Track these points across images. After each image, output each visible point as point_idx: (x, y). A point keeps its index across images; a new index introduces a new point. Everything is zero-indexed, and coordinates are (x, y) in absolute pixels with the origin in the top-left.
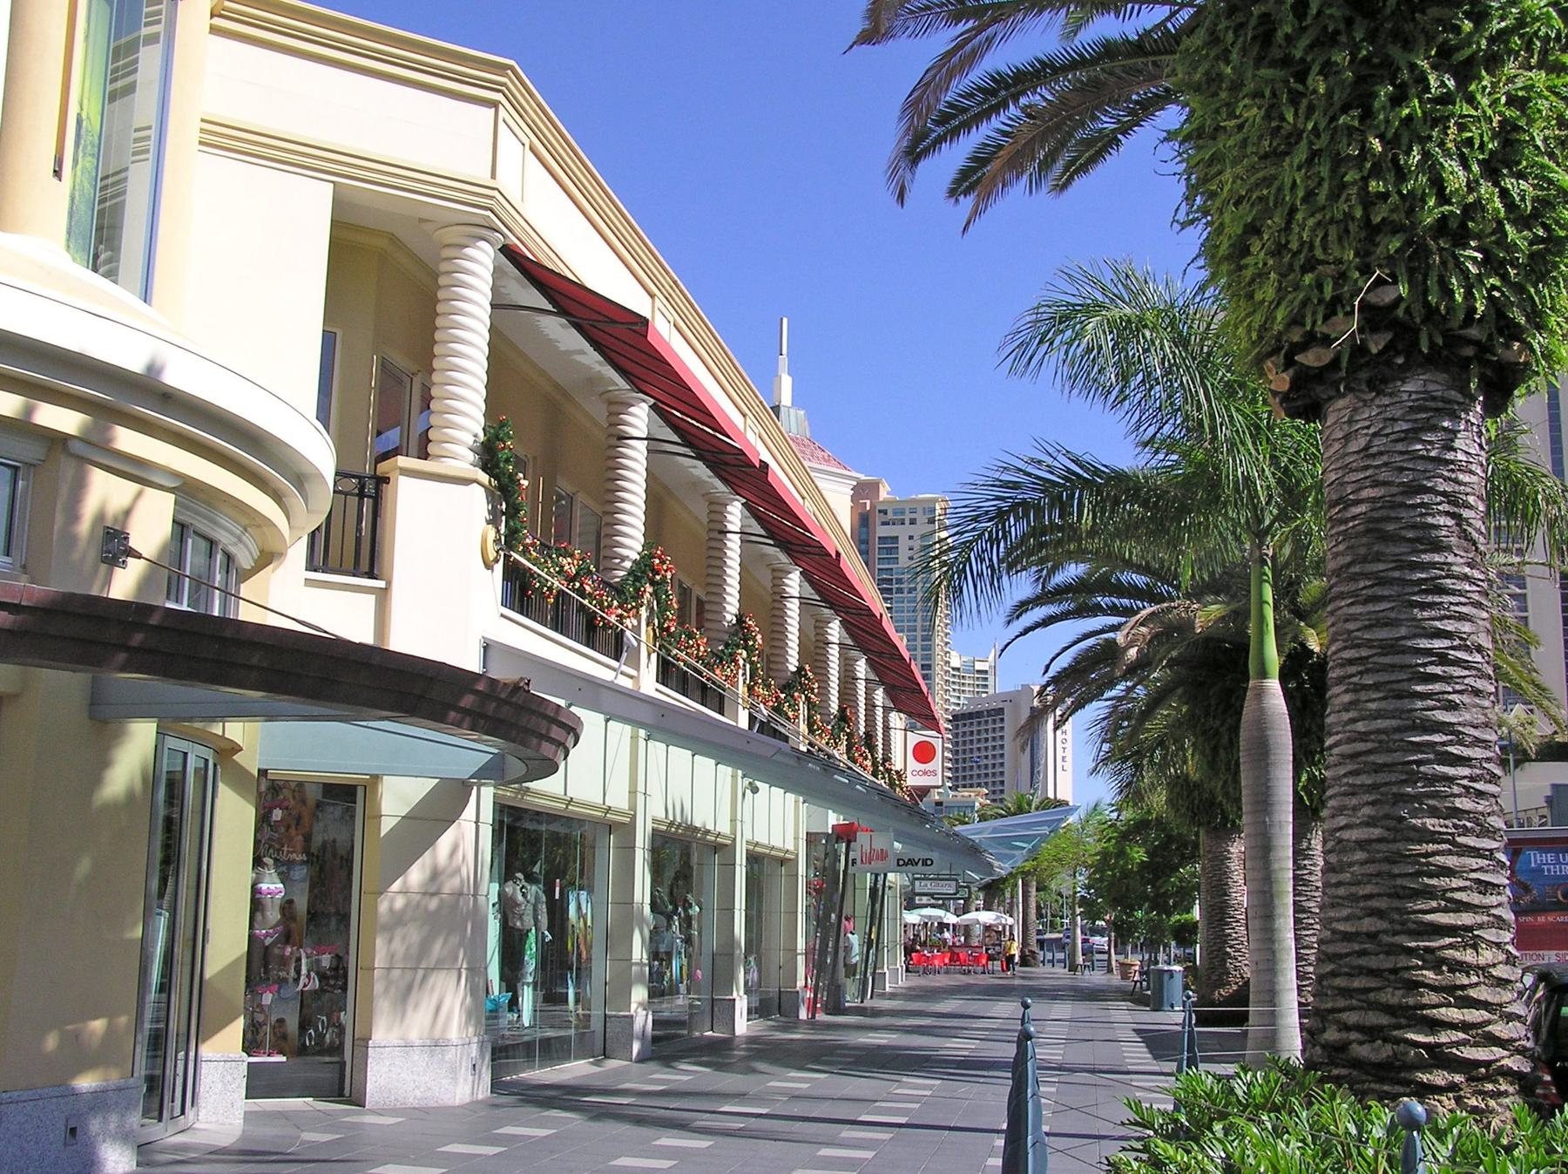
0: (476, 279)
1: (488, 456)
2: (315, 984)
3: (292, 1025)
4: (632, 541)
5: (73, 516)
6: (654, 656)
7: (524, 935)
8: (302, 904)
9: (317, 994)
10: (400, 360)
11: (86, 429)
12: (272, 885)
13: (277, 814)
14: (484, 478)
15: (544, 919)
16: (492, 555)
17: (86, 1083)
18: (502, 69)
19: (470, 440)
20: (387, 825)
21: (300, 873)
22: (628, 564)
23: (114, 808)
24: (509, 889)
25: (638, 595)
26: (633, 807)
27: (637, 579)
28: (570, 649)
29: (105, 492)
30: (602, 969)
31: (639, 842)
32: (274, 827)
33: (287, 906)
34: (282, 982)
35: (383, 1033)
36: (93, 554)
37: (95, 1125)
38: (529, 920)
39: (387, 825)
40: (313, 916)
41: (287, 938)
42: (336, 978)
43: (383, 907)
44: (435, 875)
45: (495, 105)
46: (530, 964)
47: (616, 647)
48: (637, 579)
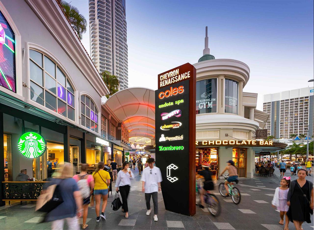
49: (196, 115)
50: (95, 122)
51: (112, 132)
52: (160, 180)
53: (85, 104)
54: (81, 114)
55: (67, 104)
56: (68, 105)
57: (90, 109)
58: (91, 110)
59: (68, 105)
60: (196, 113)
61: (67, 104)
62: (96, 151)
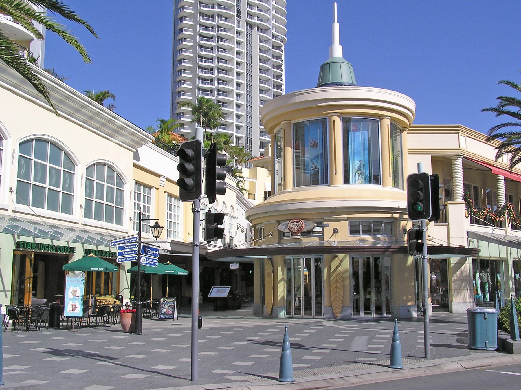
0: (459, 165)
1: (465, 198)
2: (443, 293)
3: (440, 300)
4: (503, 200)
5: (400, 227)
6: (510, 225)
7: (485, 283)
8: (439, 279)
9: (444, 294)
10: (447, 178)
11: (400, 216)
12: (434, 276)
13: (434, 264)
14: (464, 202)
15: (490, 280)
16: (467, 216)
17: (409, 304)
18: (458, 126)
19: (461, 195)
20: (452, 265)
21: (439, 274)
22: (502, 206)
23: (409, 266)
24: (481, 274)
25: (504, 214)
26: (507, 256)
27: (504, 210)
28: (240, 381)
29: (403, 223)
30: (503, 289)
31: (509, 263)
32: (433, 266)
33: (437, 280)
34: (437, 293)
35: (454, 300)
36: (402, 232)
37: (411, 309)
38: (486, 280)
39: (452, 265)
40: (442, 281)
41: (438, 285)
42: (446, 291)
43: (453, 278)
44: (462, 272)
45: (458, 133)
46: (487, 289)
47: (501, 225)
48: (504, 210)
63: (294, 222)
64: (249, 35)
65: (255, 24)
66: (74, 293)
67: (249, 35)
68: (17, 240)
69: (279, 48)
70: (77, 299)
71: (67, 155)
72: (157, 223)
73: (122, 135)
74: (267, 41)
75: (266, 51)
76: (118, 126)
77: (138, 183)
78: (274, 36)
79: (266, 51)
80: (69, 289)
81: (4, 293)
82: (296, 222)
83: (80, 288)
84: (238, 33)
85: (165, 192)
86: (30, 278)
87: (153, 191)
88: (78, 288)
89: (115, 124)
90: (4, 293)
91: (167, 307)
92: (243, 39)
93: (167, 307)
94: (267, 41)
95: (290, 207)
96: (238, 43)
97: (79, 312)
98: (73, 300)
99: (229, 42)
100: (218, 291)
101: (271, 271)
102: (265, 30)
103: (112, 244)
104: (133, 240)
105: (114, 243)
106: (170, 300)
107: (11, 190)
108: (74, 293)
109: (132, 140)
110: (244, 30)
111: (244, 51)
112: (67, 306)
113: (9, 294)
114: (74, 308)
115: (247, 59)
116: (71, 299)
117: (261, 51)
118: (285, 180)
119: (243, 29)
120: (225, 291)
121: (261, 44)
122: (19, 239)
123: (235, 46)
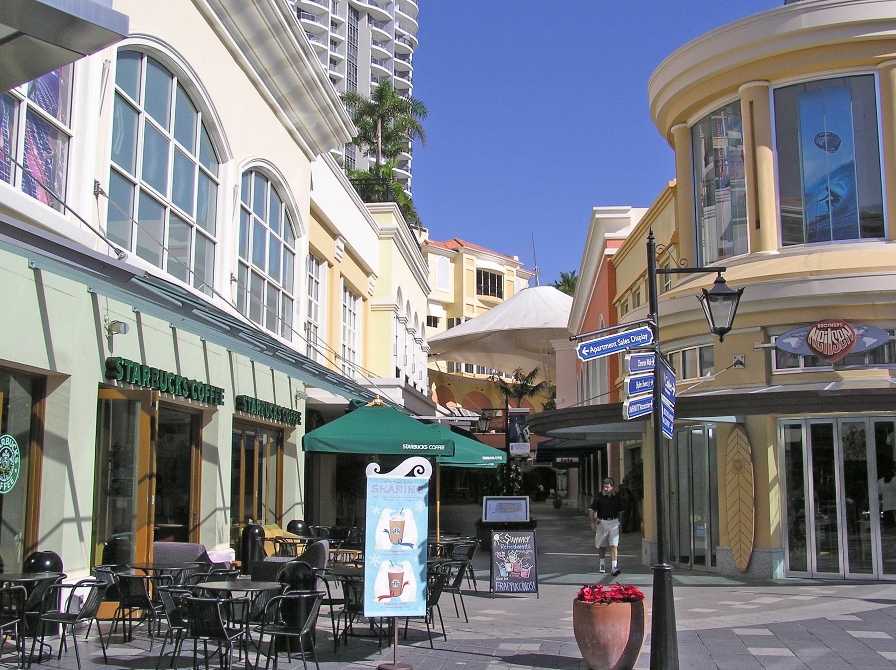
49: (484, 520)
50: (284, 287)
51: (344, 327)
52: (441, 307)
53: (141, 108)
54: (112, 168)
55: (196, 226)
56: (197, 230)
57: (265, 229)
58: (147, 122)
59: (197, 230)
60: (292, 655)
61: (196, 226)
62: (837, 569)
63: (825, 329)
64: (353, 30)
65: (365, 10)
66: (396, 533)
67: (353, 30)
68: (107, 355)
69: (404, 57)
70: (405, 555)
71: (208, 128)
72: (720, 281)
73: (305, 108)
74: (385, 42)
75: (384, 60)
76: (304, 77)
77: (736, 105)
78: (399, 36)
79: (384, 60)
80: (379, 517)
81: (75, 525)
82: (833, 329)
83: (415, 513)
84: (335, 24)
85: (342, 275)
86: (150, 477)
87: (324, 266)
88: (408, 512)
89: (301, 71)
90: (75, 525)
91: (513, 558)
92: (343, 37)
93: (513, 558)
94: (385, 42)
95: (817, 289)
96: (334, 43)
97: (412, 601)
98: (393, 557)
99: (318, 40)
100: (500, 508)
101: (749, 458)
102: (384, 23)
103: (584, 352)
104: (639, 338)
105: (588, 347)
106: (519, 539)
107: (98, 192)
108: (396, 533)
109: (318, 128)
110: (345, 20)
111: (344, 57)
112: (374, 579)
113: (87, 527)
114: (396, 585)
115: (349, 74)
116: (384, 555)
117: (374, 61)
118: (758, 225)
119: (344, 18)
120: (519, 508)
121: (374, 47)
122: (112, 352)
123: (328, 47)
